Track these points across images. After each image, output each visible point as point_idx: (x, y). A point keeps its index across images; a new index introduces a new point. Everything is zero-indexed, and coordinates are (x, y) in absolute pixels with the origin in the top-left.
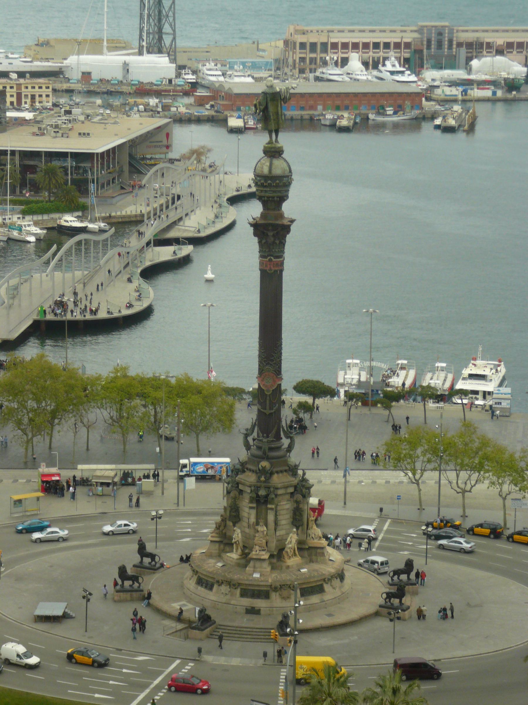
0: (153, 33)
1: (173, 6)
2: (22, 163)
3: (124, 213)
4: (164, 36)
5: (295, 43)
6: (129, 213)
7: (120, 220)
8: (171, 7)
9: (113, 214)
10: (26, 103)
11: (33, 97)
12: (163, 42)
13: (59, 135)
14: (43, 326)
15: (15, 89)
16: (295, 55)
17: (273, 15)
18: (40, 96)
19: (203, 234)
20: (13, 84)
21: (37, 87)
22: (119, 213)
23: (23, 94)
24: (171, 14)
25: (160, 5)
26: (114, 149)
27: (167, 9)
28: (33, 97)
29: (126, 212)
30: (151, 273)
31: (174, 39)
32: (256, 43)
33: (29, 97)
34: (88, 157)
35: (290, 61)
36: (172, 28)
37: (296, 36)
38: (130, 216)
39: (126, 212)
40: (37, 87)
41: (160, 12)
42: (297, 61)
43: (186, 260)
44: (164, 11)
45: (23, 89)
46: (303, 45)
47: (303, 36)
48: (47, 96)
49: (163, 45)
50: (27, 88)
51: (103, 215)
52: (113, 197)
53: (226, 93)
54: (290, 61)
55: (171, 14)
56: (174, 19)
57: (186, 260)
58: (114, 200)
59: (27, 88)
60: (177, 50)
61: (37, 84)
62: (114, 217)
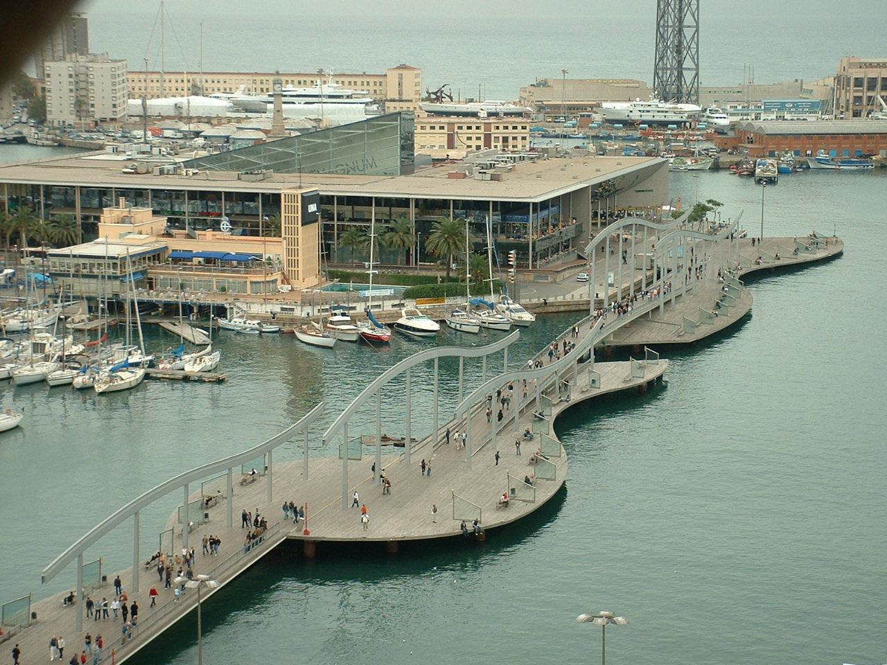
0: (671, 69)
1: (696, 35)
2: (419, 219)
3: (568, 298)
4: (684, 72)
5: (849, 79)
6: (577, 298)
7: (562, 309)
8: (693, 38)
9: (551, 300)
10: (496, 147)
11: (505, 140)
12: (683, 80)
13: (488, 177)
14: (310, 551)
15: (482, 130)
16: (848, 94)
17: (844, 522)
18: (515, 138)
19: (689, 338)
20: (480, 123)
21: (510, 127)
22: (560, 299)
23: (493, 136)
24: (693, 45)
25: (680, 34)
26: (568, 195)
27: (688, 38)
28: (505, 140)
29: (573, 295)
30: (574, 419)
31: (697, 75)
32: (799, 82)
33: (501, 139)
34: (520, 208)
35: (843, 103)
36: (694, 63)
37: (850, 70)
38: (578, 304)
39: (573, 295)
40: (510, 127)
41: (680, 43)
42: (851, 101)
43: (654, 389)
44: (685, 41)
45: (493, 130)
46: (859, 82)
47: (858, 70)
48: (524, 138)
49: (683, 83)
50: (498, 128)
51: (535, 301)
52: (557, 272)
53: (755, 134)
54: (843, 103)
55: (693, 45)
56: (697, 51)
57: (654, 389)
58: (559, 277)
59: (498, 128)
60: (700, 90)
61: (511, 123)
62: (552, 305)
